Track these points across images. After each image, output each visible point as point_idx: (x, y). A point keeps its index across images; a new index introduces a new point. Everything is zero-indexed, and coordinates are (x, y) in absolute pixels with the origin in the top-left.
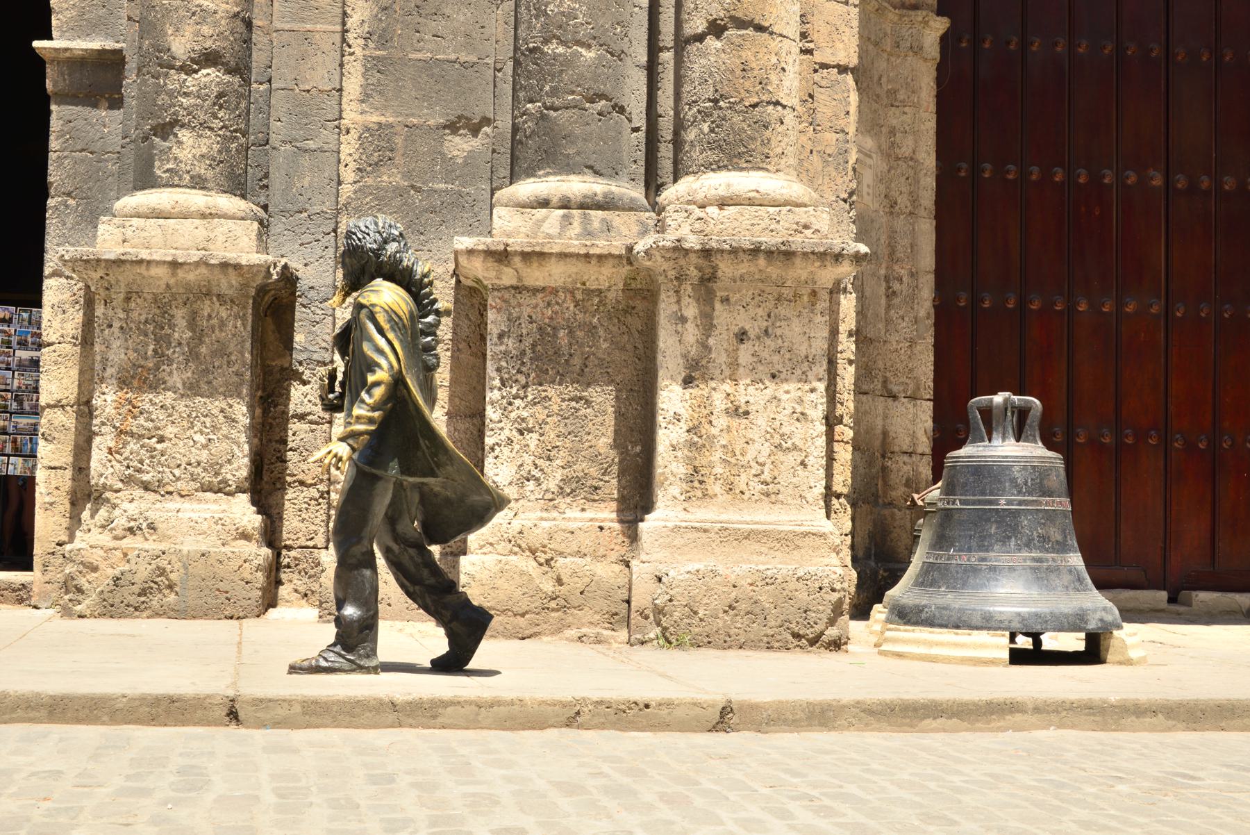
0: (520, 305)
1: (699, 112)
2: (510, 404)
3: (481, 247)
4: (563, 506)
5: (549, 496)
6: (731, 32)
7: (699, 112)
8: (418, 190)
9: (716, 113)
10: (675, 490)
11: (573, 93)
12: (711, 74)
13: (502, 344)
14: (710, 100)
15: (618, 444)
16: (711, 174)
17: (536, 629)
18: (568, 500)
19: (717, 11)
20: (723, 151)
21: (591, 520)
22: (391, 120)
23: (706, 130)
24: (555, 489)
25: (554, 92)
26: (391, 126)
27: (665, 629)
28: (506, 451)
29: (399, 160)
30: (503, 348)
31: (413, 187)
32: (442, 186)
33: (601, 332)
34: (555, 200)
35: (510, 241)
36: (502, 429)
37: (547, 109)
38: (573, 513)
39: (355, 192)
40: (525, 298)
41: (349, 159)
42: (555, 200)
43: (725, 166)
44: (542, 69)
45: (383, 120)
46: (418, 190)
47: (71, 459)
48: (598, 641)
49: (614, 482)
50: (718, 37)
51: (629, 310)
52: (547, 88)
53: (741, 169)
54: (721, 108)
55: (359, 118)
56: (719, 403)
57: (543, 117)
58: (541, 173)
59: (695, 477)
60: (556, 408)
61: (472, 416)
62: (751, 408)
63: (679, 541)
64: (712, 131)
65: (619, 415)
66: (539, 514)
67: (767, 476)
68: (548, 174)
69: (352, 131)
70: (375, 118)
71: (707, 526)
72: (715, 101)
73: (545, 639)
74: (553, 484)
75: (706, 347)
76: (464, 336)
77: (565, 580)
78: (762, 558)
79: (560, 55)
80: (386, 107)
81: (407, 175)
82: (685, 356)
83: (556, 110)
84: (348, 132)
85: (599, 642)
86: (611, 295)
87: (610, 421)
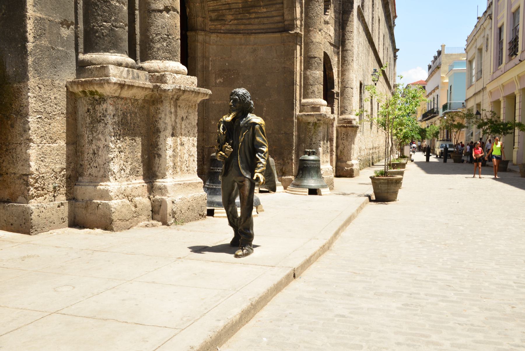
0: (118, 104)
1: (161, 38)
2: (117, 142)
3: (119, 82)
4: (131, 179)
5: (127, 176)
6: (172, 12)
7: (161, 38)
8: (54, 49)
9: (168, 40)
10: (170, 171)
11: (122, 22)
12: (166, 26)
13: (114, 119)
14: (166, 35)
15: (142, 156)
16: (167, 61)
17: (131, 225)
18: (132, 176)
19: (168, 4)
20: (171, 54)
21: (139, 183)
22: (44, 16)
23: (165, 45)
24: (129, 173)
25: (116, 20)
26: (44, 19)
27: (176, 219)
28: (116, 159)
29: (47, 35)
30: (114, 120)
31: (52, 47)
32: (61, 48)
33: (138, 115)
34: (124, 64)
35: (126, 80)
36: (115, 151)
37: (113, 26)
38: (134, 181)
39: (33, 47)
40: (120, 102)
41: (31, 32)
42: (124, 64)
43: (172, 59)
44: (110, 10)
45: (41, 16)
46: (54, 49)
47: (64, 165)
48: (153, 226)
49: (142, 169)
50: (167, 13)
51: (143, 107)
52: (113, 18)
53: (176, 61)
54: (169, 38)
55: (33, 13)
56: (179, 142)
57: (112, 29)
58: (112, 51)
59: (174, 167)
60: (128, 143)
61: (73, 144)
62: (185, 143)
63: (175, 189)
64: (167, 46)
65: (142, 145)
66: (127, 183)
67: (187, 165)
68: (114, 52)
69: (31, 19)
70: (39, 15)
71: (181, 183)
72: (168, 35)
73: (135, 228)
74: (128, 171)
75: (176, 122)
76: (70, 111)
77: (138, 206)
78: (191, 192)
79: (117, 6)
80: (42, 10)
81: (50, 42)
82: (172, 125)
83: (117, 28)
84: (29, 19)
85: (154, 226)
86: (140, 101)
87: (140, 146)
